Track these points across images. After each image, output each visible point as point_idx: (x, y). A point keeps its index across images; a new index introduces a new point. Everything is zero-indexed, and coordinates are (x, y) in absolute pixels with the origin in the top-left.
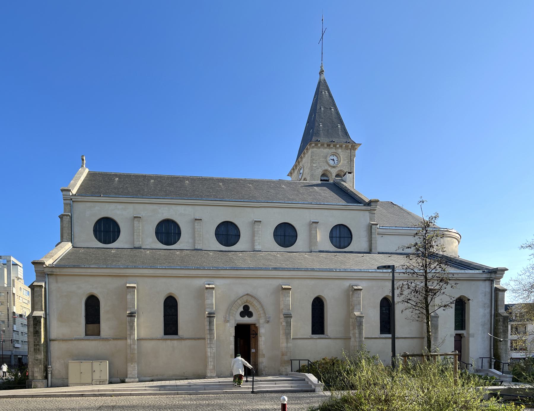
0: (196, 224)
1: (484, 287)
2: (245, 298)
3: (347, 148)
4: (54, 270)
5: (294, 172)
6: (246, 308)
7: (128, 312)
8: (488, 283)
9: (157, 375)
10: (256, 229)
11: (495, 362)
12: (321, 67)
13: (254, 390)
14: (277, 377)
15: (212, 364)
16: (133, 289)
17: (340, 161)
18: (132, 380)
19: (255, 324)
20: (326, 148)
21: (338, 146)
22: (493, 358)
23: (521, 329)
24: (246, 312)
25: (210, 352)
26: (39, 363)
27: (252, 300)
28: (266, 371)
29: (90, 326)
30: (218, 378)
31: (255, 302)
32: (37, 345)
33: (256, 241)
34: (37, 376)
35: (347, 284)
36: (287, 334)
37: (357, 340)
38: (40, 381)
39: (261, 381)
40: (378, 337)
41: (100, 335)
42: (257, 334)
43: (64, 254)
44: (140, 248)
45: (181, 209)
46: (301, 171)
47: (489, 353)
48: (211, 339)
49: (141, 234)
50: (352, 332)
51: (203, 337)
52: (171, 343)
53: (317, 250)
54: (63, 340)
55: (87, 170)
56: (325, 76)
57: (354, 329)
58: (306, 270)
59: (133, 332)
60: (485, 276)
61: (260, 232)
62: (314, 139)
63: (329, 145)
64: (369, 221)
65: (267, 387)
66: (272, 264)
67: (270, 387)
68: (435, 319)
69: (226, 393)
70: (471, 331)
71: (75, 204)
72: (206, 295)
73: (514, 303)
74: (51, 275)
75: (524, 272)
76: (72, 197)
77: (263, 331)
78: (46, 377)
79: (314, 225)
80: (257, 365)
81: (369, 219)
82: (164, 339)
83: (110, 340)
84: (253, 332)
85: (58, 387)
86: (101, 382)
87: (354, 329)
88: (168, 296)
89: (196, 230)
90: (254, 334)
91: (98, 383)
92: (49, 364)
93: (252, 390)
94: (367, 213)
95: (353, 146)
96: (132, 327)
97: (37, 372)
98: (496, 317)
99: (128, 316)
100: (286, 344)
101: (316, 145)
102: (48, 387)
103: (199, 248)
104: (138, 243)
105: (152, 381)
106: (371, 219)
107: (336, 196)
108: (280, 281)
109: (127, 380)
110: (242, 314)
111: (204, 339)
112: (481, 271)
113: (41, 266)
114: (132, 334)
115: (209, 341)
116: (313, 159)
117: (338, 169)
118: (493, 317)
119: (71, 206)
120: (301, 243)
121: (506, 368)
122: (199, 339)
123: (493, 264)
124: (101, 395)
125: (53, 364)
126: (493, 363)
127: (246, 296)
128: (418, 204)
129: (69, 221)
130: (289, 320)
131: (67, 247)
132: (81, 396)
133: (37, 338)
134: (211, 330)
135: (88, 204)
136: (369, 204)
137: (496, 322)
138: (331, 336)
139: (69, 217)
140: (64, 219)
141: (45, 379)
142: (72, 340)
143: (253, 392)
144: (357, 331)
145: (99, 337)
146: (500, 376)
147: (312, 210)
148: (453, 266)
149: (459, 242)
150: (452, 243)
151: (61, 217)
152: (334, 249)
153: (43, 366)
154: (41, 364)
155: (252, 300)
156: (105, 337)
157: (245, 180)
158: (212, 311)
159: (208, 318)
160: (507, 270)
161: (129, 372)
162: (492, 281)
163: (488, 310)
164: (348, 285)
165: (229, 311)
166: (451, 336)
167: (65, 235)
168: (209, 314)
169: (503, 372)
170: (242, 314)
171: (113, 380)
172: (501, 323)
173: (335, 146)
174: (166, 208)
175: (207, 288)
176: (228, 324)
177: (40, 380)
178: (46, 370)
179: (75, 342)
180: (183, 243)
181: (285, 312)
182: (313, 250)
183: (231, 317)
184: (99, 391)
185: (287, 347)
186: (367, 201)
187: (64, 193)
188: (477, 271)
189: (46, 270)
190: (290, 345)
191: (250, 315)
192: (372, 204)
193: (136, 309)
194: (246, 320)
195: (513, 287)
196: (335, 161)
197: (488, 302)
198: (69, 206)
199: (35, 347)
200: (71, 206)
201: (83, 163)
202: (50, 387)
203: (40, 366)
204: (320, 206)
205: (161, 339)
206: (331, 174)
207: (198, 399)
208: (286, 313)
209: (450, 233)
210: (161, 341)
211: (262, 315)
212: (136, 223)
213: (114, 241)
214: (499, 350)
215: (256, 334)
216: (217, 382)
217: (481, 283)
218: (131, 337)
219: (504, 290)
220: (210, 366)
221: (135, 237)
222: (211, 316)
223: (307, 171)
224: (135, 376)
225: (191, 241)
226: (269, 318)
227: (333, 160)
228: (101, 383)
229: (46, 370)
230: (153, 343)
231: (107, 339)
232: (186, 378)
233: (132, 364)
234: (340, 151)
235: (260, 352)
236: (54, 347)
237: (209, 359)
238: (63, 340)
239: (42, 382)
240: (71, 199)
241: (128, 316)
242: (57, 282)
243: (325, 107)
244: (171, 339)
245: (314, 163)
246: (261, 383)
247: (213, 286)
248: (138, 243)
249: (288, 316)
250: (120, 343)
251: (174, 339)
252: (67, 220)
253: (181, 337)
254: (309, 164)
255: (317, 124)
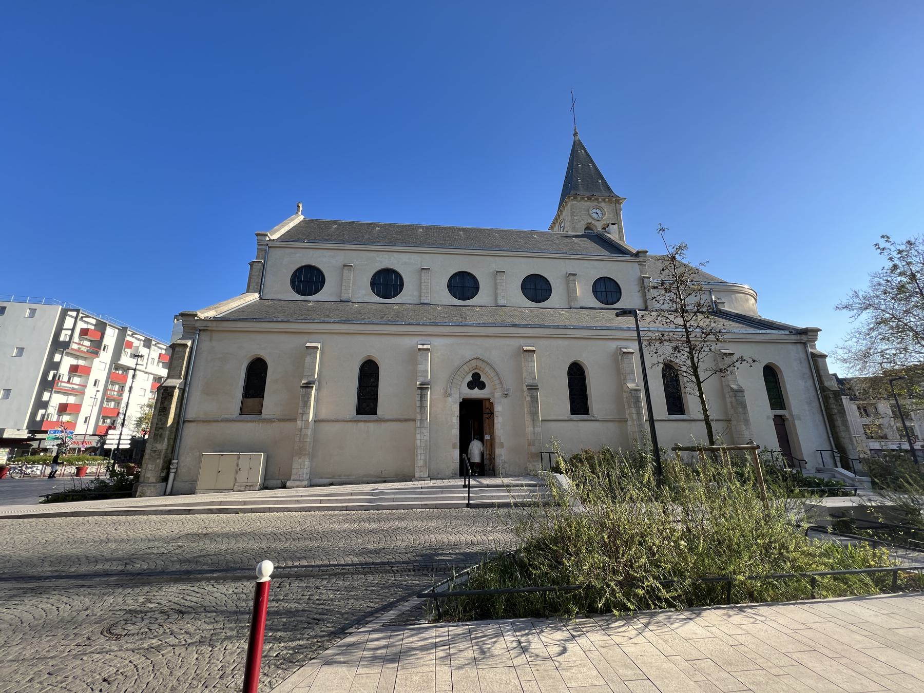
0: (423, 275)
1: (795, 352)
2: (474, 363)
3: (610, 201)
4: (209, 324)
5: (555, 226)
6: (476, 376)
7: (303, 382)
8: (799, 347)
9: (340, 476)
10: (498, 281)
11: (840, 457)
12: (575, 130)
13: (470, 502)
14: (519, 480)
15: (423, 457)
16: (315, 350)
17: (605, 214)
18: (298, 483)
19: (489, 399)
20: (586, 201)
21: (600, 199)
22: (836, 451)
23: (871, 410)
24: (476, 382)
25: (421, 439)
26: (157, 457)
27: (483, 365)
28: (507, 469)
29: (250, 401)
30: (431, 479)
31: (487, 369)
32: (160, 428)
33: (499, 295)
34: (149, 478)
35: (613, 345)
36: (534, 414)
37: (635, 423)
38: (153, 484)
39: (488, 486)
40: (667, 419)
41: (261, 414)
42: (492, 413)
43: (241, 306)
44: (349, 301)
45: (405, 257)
46: (563, 225)
47: (828, 443)
48: (422, 421)
49: (351, 285)
50: (627, 412)
51: (412, 417)
52: (367, 428)
53: (578, 307)
54: (204, 421)
55: (301, 218)
56: (579, 137)
57: (630, 407)
58: (558, 327)
59: (308, 410)
60: (794, 337)
61: (504, 284)
62: (572, 192)
63: (589, 199)
64: (639, 274)
65: (495, 496)
66: (514, 321)
67: (498, 497)
68: (740, 394)
69: (425, 507)
70: (795, 412)
71: (271, 250)
72: (419, 358)
73: (849, 376)
74: (204, 330)
75: (849, 337)
76: (268, 243)
77: (501, 409)
78: (165, 479)
79: (572, 277)
80: (494, 458)
81: (639, 271)
82: (355, 421)
83: (275, 421)
84: (488, 411)
85: (181, 494)
86: (249, 487)
87: (630, 407)
88: (364, 361)
89: (423, 281)
90: (488, 413)
91: (243, 488)
92: (176, 457)
93: (467, 502)
94: (636, 265)
95: (618, 201)
96: (306, 404)
97: (151, 470)
98: (824, 392)
99: (302, 387)
100: (532, 428)
101: (575, 198)
102: (165, 495)
103: (426, 302)
104: (346, 295)
105: (331, 484)
106: (641, 272)
107: (599, 247)
108: (522, 341)
109: (288, 484)
110: (471, 386)
111: (414, 420)
112: (787, 332)
113: (191, 319)
114: (306, 412)
115: (419, 424)
116: (574, 212)
117: (604, 222)
118: (819, 392)
119: (266, 253)
120: (556, 298)
121: (858, 467)
122: (406, 420)
123: (802, 325)
124: (220, 511)
125: (182, 458)
126: (838, 459)
127: (475, 361)
128: (658, 233)
129: (260, 269)
130: (535, 394)
131: (254, 297)
132: (188, 513)
133: (162, 418)
134: (422, 407)
135: (288, 251)
136: (637, 254)
137: (826, 399)
138: (599, 418)
139: (260, 264)
140: (254, 267)
141: (163, 482)
142: (217, 421)
143: (468, 505)
144: (633, 410)
145: (258, 417)
146: (853, 479)
147: (567, 261)
148: (751, 326)
149: (756, 300)
150: (747, 300)
151: (251, 264)
152: (598, 305)
153: (162, 461)
154: (159, 458)
155: (483, 365)
156: (268, 417)
157: (491, 230)
158: (426, 381)
159: (419, 391)
160: (820, 330)
161: (294, 471)
162: (805, 344)
163: (810, 383)
164: (615, 347)
165: (451, 380)
166: (768, 417)
167: (253, 285)
168: (421, 384)
169: (855, 473)
170: (471, 386)
171: (271, 483)
172: (832, 401)
173: (597, 199)
174: (386, 255)
175: (420, 349)
176: (450, 399)
177: (153, 483)
178: (167, 467)
179: (222, 425)
180: (407, 296)
181: (529, 381)
182: (573, 307)
183: (454, 390)
184: (221, 503)
185: (534, 433)
186: (634, 252)
187: (259, 237)
188: (782, 332)
189: (198, 325)
190: (538, 429)
191: (482, 386)
192: (640, 255)
193: (316, 377)
194: (476, 393)
195: (843, 355)
196: (599, 215)
197: (807, 371)
198: (263, 252)
199: (156, 432)
200: (266, 253)
201: (299, 210)
202: (169, 495)
203: (158, 461)
204: (576, 254)
205: (350, 421)
206: (596, 227)
207: (369, 520)
208: (530, 384)
209: (741, 289)
210: (350, 424)
211: (498, 386)
212: (346, 272)
213: (316, 292)
214: (842, 439)
215: (491, 413)
216: (419, 488)
217: (790, 347)
218: (304, 418)
219: (824, 356)
220: (419, 461)
221: (343, 288)
222: (423, 388)
223: (568, 224)
224: (303, 477)
225: (416, 293)
226: (508, 390)
227: (597, 213)
228: (248, 488)
229: (167, 467)
230: (338, 426)
231: (269, 421)
232: (384, 479)
233: (300, 458)
234: (603, 204)
235: (497, 440)
236: (190, 433)
237: (419, 450)
238: (204, 421)
239: (154, 486)
240: (267, 245)
241: (302, 387)
242: (211, 340)
243: (582, 164)
244: (365, 421)
245: (574, 216)
246: (487, 490)
247: (429, 347)
248: (346, 295)
249: (533, 388)
250: (288, 426)
251: (370, 421)
252: (258, 267)
253: (381, 417)
254: (570, 218)
255: (574, 179)
